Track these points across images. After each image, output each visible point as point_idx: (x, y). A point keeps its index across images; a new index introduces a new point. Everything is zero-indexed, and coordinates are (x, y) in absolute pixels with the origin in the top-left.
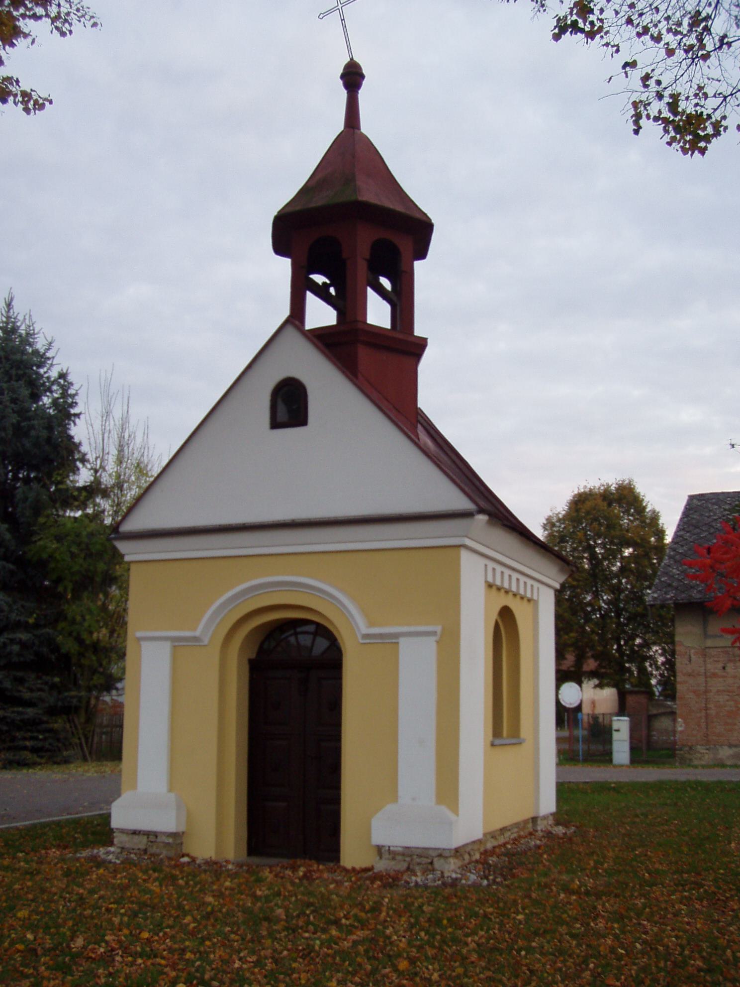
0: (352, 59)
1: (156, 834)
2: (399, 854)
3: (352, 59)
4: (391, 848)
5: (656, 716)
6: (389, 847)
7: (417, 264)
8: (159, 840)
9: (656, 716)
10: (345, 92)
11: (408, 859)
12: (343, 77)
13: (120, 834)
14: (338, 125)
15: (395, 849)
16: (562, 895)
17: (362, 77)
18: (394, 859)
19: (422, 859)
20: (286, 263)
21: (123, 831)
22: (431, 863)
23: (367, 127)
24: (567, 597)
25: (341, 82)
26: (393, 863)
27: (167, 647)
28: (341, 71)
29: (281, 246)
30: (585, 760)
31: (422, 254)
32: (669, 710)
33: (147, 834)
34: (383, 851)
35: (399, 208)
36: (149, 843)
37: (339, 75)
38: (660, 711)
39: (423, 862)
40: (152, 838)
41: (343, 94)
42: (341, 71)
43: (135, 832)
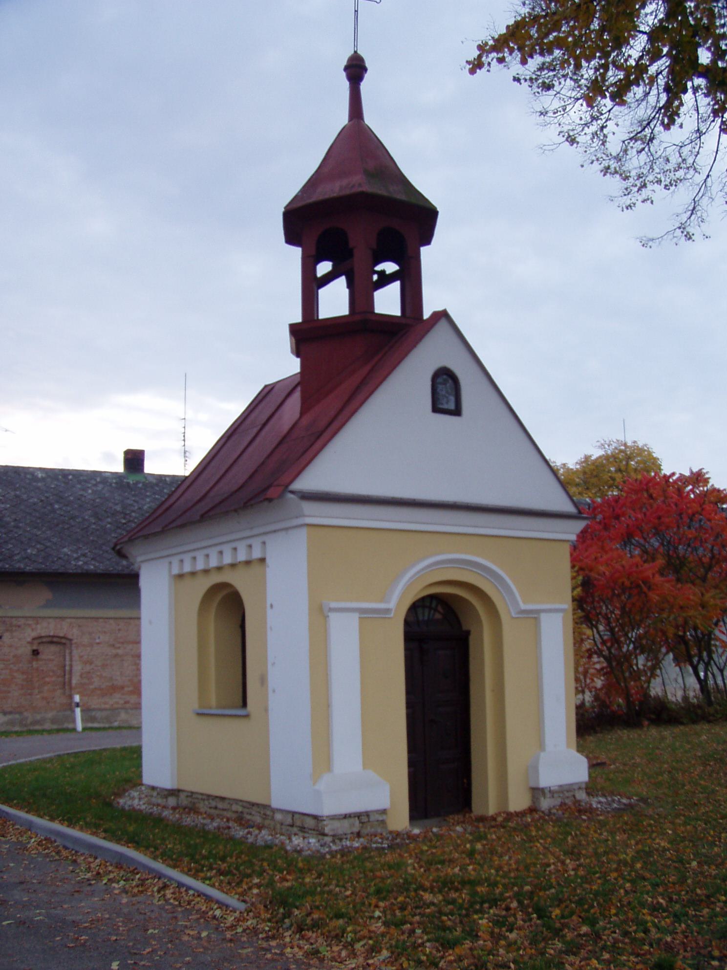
0: (356, 52)
1: (367, 814)
2: (557, 792)
3: (356, 52)
4: (552, 788)
7: (387, 273)
12: (346, 69)
13: (331, 822)
14: (342, 119)
16: (100, 915)
17: (366, 70)
20: (297, 252)
21: (333, 818)
23: (370, 119)
24: (698, 492)
25: (344, 74)
28: (345, 63)
29: (292, 238)
31: (427, 238)
33: (358, 815)
35: (402, 197)
37: (343, 67)
40: (364, 819)
41: (346, 84)
42: (344, 63)
43: (346, 817)
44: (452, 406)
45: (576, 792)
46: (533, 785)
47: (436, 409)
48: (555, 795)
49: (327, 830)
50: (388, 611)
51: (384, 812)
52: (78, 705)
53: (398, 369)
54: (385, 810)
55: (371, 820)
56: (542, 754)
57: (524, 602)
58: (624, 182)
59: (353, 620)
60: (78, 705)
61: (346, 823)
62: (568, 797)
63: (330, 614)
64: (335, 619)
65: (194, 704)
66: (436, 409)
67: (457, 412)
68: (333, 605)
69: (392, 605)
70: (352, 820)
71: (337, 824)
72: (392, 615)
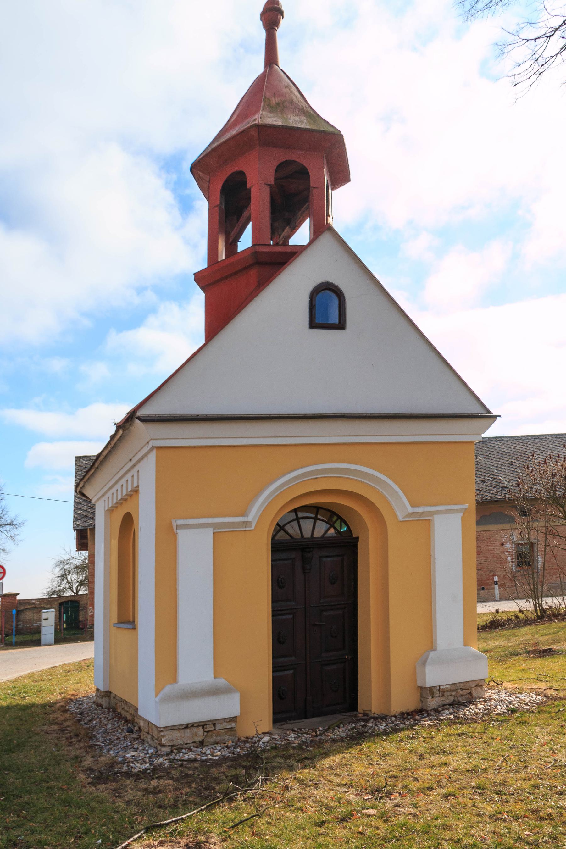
1: (214, 723)
5: (22, 611)
6: (439, 686)
8: (218, 727)
9: (22, 611)
10: (264, 31)
11: (454, 693)
12: (263, 15)
13: (169, 732)
15: (445, 687)
18: (443, 696)
19: (464, 691)
21: (172, 728)
22: (470, 693)
26: (443, 699)
27: (208, 534)
28: (261, 9)
30: (15, 646)
32: (33, 606)
33: (203, 725)
34: (434, 691)
36: (206, 733)
38: (26, 608)
39: (465, 694)
40: (210, 728)
44: (334, 319)
45: (473, 689)
46: (420, 684)
47: (313, 325)
48: (447, 694)
49: (164, 741)
50: (246, 523)
51: (234, 719)
52: (496, 583)
53: (215, 338)
54: (235, 717)
55: (217, 728)
56: (432, 654)
57: (412, 506)
58: (5, 548)
59: (207, 536)
60: (496, 583)
61: (188, 732)
62: (462, 695)
63: (178, 531)
64: (183, 536)
65: (115, 619)
66: (313, 325)
67: (341, 326)
68: (180, 522)
69: (253, 516)
70: (195, 730)
71: (176, 734)
72: (253, 528)
